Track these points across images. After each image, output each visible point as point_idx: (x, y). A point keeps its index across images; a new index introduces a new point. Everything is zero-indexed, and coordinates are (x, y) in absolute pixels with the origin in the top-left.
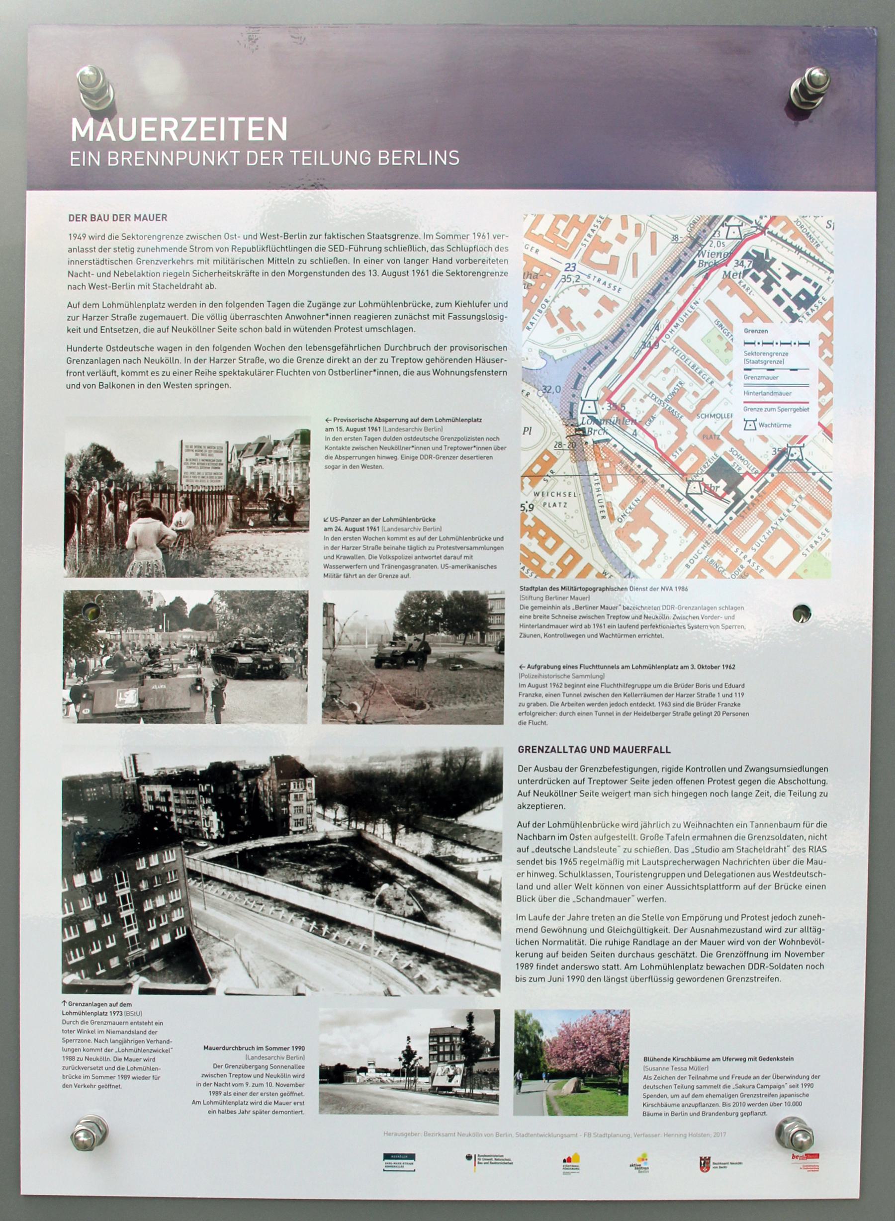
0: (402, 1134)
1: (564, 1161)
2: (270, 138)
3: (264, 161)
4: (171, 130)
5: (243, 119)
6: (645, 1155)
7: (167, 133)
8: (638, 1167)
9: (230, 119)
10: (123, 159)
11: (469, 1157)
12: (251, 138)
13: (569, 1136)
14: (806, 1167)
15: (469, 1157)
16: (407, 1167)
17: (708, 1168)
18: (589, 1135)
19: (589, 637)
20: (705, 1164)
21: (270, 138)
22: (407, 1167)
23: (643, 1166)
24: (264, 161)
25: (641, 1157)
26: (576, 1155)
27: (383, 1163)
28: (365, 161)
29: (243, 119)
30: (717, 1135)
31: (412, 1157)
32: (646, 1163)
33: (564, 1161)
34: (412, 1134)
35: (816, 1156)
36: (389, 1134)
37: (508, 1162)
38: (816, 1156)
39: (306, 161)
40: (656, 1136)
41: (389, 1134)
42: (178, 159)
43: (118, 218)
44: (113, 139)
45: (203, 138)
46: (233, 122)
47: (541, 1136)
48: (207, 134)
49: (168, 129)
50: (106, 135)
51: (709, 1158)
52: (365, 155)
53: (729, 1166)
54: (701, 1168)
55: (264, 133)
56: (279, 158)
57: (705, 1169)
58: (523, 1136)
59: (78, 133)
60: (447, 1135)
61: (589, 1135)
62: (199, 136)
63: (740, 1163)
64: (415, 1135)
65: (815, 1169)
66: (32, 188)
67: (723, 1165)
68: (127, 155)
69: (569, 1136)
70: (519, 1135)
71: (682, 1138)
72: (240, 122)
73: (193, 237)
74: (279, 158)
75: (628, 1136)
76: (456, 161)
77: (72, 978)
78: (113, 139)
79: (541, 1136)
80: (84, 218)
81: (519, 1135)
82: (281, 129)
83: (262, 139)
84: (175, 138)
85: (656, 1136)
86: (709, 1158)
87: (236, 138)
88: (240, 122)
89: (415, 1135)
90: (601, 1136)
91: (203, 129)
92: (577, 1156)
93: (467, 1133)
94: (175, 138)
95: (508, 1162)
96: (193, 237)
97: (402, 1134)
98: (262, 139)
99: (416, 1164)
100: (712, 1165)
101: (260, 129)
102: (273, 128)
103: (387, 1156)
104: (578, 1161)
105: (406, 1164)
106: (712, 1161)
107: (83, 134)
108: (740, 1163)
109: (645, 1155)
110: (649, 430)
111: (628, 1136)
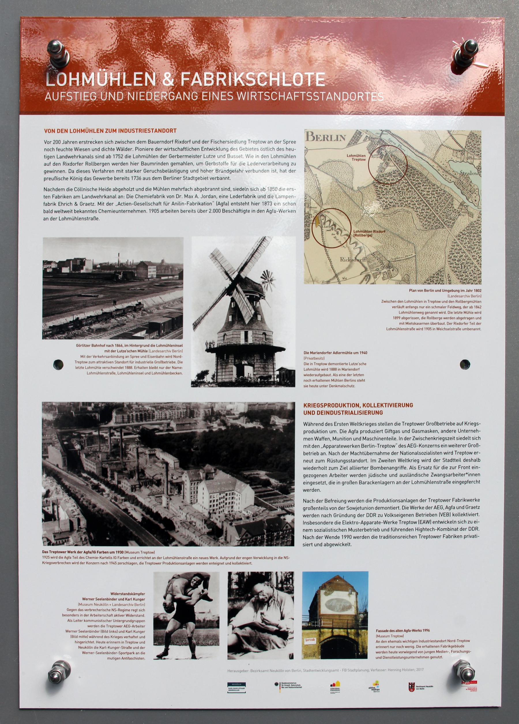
0: (238, 671)
1: (331, 686)
2: (146, 84)
3: (142, 98)
4: (223, 80)
5: (313, 73)
6: (377, 682)
7: (220, 82)
8: (373, 689)
9: (306, 73)
10: (252, 96)
11: (276, 684)
12: (317, 85)
13: (334, 671)
14: (469, 689)
15: (276, 684)
16: (241, 691)
17: (414, 690)
18: (345, 670)
19: (146, 374)
20: (412, 687)
21: (146, 84)
22: (241, 691)
23: (376, 688)
24: (142, 98)
25: (375, 682)
26: (338, 682)
27: (227, 688)
28: (171, 98)
29: (313, 73)
30: (418, 669)
31: (244, 684)
32: (378, 687)
33: (331, 686)
34: (244, 671)
35: (476, 682)
36: (231, 671)
37: (299, 687)
38: (476, 682)
39: (204, 98)
40: (383, 670)
41: (231, 671)
42: (61, 96)
43: (60, 131)
44: (201, 85)
45: (135, 84)
46: (307, 75)
47: (318, 671)
48: (138, 82)
49: (221, 79)
50: (197, 82)
51: (414, 683)
52: (194, 95)
53: (425, 688)
54: (410, 690)
55: (143, 82)
56: (254, 96)
57: (412, 690)
58: (308, 671)
59: (85, 81)
60: (264, 671)
61: (345, 670)
62: (133, 84)
63: (432, 686)
64: (246, 671)
65: (474, 690)
66: (22, 113)
67: (422, 688)
68: (254, 94)
69: (334, 671)
70: (305, 671)
71: (399, 672)
72: (311, 75)
73: (119, 142)
74: (254, 96)
75: (368, 671)
76: (231, 98)
77: (235, 578)
78: (201, 85)
79: (318, 671)
80: (66, 131)
81: (305, 671)
82: (148, 79)
83: (141, 85)
84: (225, 84)
85: (383, 670)
86: (414, 683)
87: (309, 85)
88: (311, 75)
89: (246, 671)
90: (352, 671)
91: (135, 79)
92: (338, 683)
93: (275, 670)
94: (225, 84)
95: (299, 687)
96: (119, 142)
97: (238, 671)
98: (141, 85)
99: (246, 689)
100: (415, 688)
101: (140, 79)
102: (152, 79)
103: (230, 684)
104: (339, 686)
105: (241, 689)
106: (416, 685)
107: (88, 82)
108: (432, 686)
109: (377, 682)
110: (329, 253)
111: (368, 671)
